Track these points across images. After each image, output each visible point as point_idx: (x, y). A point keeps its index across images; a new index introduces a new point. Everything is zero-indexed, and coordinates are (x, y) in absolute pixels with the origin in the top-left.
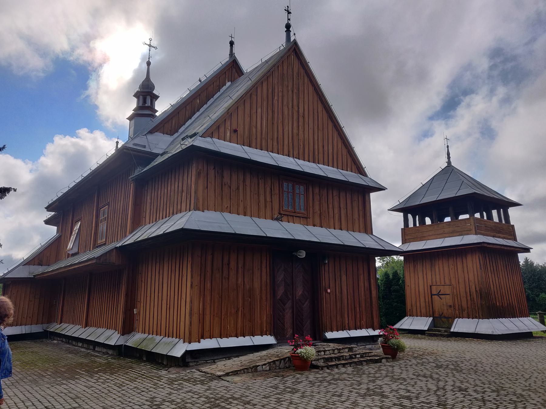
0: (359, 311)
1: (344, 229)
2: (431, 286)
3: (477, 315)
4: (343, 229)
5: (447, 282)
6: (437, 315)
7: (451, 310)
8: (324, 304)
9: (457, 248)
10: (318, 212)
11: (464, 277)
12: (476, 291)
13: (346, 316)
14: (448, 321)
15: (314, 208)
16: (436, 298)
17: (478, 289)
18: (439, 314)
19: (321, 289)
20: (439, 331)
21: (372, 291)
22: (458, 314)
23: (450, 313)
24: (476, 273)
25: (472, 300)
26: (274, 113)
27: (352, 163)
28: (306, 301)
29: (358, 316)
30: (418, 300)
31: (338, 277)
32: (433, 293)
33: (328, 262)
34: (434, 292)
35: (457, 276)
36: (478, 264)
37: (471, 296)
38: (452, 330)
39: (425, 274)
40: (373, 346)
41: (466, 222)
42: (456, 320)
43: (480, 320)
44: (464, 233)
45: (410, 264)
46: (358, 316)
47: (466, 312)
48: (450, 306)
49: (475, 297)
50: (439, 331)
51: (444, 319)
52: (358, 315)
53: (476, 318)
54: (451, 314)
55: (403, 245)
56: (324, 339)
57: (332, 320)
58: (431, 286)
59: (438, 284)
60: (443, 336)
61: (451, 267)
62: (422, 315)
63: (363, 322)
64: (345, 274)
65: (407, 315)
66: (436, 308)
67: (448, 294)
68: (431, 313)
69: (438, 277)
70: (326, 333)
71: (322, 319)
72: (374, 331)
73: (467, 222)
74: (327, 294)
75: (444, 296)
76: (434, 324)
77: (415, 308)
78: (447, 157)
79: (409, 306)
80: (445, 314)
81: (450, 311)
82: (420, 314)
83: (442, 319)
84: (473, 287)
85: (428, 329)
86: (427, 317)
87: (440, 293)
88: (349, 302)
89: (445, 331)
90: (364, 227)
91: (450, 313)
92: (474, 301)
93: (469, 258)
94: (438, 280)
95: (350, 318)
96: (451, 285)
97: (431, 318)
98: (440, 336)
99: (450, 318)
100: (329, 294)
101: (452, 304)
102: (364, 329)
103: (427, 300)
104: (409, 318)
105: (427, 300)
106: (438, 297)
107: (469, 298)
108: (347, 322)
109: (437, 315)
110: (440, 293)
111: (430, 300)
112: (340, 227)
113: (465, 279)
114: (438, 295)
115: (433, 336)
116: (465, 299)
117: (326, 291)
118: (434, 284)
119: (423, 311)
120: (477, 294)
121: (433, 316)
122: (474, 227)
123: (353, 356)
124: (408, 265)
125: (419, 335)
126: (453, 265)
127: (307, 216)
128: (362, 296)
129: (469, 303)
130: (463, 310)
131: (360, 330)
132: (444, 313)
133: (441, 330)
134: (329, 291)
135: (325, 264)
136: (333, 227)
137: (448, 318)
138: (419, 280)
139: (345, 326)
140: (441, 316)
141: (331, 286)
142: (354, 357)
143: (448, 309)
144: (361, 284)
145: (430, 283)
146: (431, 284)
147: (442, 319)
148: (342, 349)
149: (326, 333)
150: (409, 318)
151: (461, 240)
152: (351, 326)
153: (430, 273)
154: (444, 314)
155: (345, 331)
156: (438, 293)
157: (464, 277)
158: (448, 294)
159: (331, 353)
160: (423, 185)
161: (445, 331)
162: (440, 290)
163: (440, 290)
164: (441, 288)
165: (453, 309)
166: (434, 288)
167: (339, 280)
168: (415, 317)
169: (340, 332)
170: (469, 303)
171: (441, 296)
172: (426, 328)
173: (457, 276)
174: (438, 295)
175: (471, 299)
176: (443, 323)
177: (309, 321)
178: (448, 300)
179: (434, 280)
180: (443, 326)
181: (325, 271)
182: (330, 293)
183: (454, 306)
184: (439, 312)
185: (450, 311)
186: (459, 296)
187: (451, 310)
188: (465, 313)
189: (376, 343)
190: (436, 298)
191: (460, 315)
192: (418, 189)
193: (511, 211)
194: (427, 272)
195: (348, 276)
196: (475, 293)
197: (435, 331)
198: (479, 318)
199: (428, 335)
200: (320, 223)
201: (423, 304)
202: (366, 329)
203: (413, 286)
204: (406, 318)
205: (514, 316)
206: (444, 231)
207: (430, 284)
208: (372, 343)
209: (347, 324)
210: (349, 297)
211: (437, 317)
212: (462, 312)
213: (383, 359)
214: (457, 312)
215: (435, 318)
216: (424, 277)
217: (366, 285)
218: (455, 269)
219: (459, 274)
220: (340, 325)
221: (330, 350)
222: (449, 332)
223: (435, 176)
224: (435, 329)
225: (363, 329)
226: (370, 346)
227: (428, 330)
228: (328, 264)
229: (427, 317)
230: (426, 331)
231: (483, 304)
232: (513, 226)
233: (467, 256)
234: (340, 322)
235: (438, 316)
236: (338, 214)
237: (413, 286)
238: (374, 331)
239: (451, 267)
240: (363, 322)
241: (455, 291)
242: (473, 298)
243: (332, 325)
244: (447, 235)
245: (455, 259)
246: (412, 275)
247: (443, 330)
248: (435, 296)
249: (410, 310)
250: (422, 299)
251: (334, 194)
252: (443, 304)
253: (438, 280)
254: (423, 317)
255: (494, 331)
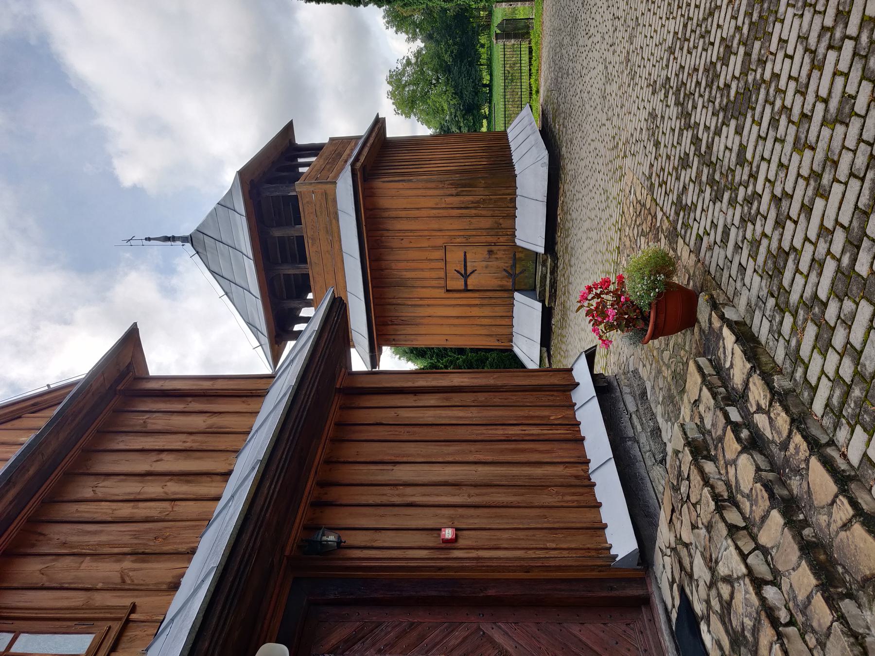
0: (520, 428)
1: (230, 464)
2: (448, 291)
3: (509, 197)
4: (231, 468)
5: (439, 254)
6: (509, 283)
7: (498, 252)
8: (500, 559)
9: (364, 224)
10: (127, 564)
11: (427, 217)
12: (457, 195)
13: (539, 471)
14: (521, 259)
15: (100, 585)
16: (472, 282)
17: (454, 191)
18: (507, 277)
19: (440, 569)
20: (544, 277)
21: (450, 384)
22: (506, 238)
23: (503, 254)
24: (420, 192)
25: (476, 205)
26: (529, 489)
27: (17, 423)
28: (491, 641)
29: (535, 431)
30: (478, 321)
31: (398, 495)
32: (463, 287)
33: (333, 529)
34: (459, 284)
35: (426, 233)
36: (400, 185)
37: (470, 206)
38: (541, 250)
39: (421, 302)
40: (626, 390)
41: (308, 202)
42: (518, 243)
43: (518, 192)
44: (332, 210)
45: (399, 333)
46: (535, 431)
47: (501, 221)
48: (490, 252)
49: (470, 198)
50: (544, 277)
51: (517, 269)
52: (531, 432)
53: (513, 201)
54: (507, 253)
55: (355, 344)
56: (638, 565)
57: (562, 525)
58: (448, 291)
59: (442, 274)
60: (556, 269)
61: (405, 243)
62: (509, 314)
63: (552, 418)
64: (390, 467)
65: (508, 348)
66: (494, 283)
67: (465, 255)
68: (505, 295)
69: (426, 274)
70: (613, 552)
71: (559, 568)
72: (578, 384)
73: (307, 200)
74: (462, 543)
75: (468, 264)
76: (529, 291)
77: (494, 329)
78: (173, 243)
79: (491, 343)
80: (506, 265)
81: (500, 255)
82: (507, 320)
83: (517, 272)
84: (449, 200)
85: (539, 301)
86: (513, 304)
87: (463, 272)
88: (490, 458)
89: (543, 266)
90: (244, 399)
91: (503, 254)
92: (478, 202)
93: (385, 202)
94: (434, 274)
95: (546, 458)
96: (445, 246)
97: (517, 295)
98: (556, 274)
99: (515, 255)
100: (460, 533)
101: (487, 248)
102: (577, 416)
103: (477, 302)
104: (515, 344)
105: (477, 302)
106: (470, 277)
107: (473, 212)
108: (559, 470)
109: (509, 283)
110: (463, 272)
111: (477, 295)
112: (219, 477)
113: (433, 215)
114: (466, 276)
115: (556, 291)
116: (474, 220)
117: (449, 545)
118: (442, 282)
119: (500, 311)
120: (465, 193)
121: (511, 290)
122: (320, 186)
123: (743, 435)
124: (402, 337)
125: (553, 322)
126: (402, 239)
127: (119, 619)
128: (470, 415)
129: (484, 212)
130: (498, 226)
131: (581, 426)
132: (504, 268)
133: (542, 274)
134: (448, 533)
135: (339, 543)
136: (211, 503)
137: (514, 258)
138: (435, 315)
139: (577, 477)
140: (511, 274)
141: (430, 523)
142: (745, 434)
143: (497, 258)
144: (429, 416)
145: (441, 293)
146: (443, 291)
147: (517, 272)
148: (713, 487)
149: (613, 552)
150: (515, 344)
151: (348, 214)
152: (572, 457)
153: (419, 290)
154: (507, 267)
155: (594, 478)
156: (463, 276)
157: (427, 217)
158: (465, 255)
159: (753, 546)
160: (226, 294)
161: (544, 264)
162: (456, 270)
163: (456, 270)
164: (451, 268)
165: (494, 248)
166: (452, 285)
167: (409, 490)
168: (514, 329)
169: (600, 494)
170: (484, 212)
171: (469, 270)
172: (539, 306)
173: (426, 233)
174: (466, 276)
175: (475, 208)
176: (525, 270)
177: (575, 629)
178: (477, 258)
179: (434, 283)
180: (533, 271)
181: (369, 544)
182: (457, 529)
183: (489, 244)
184: (503, 278)
185: (500, 255)
186: (469, 233)
187: (498, 252)
188: (506, 223)
189: (616, 384)
190: (472, 282)
191: (509, 233)
192: (235, 306)
193: (302, 138)
194: (416, 296)
195: (398, 459)
196: (462, 198)
197: (543, 285)
198: (515, 194)
199: (554, 300)
200: (175, 557)
201: (487, 311)
202: (576, 408)
203: (447, 330)
204: (516, 350)
205: (509, 147)
206: (327, 251)
207: (443, 290)
208: (618, 394)
209: (565, 471)
210: (471, 458)
211: (514, 284)
212: (502, 228)
213: (726, 316)
214: (502, 239)
215: (516, 288)
216: (427, 304)
217: (432, 402)
218: (412, 234)
219: (422, 227)
220: (574, 494)
221: (737, 548)
222: (545, 257)
223: (209, 270)
224: (541, 286)
225: (578, 420)
226: (629, 400)
227: (543, 301)
228: (342, 533)
229: (514, 305)
230: (544, 306)
231: (485, 183)
232: (332, 139)
233: (384, 208)
234: (563, 495)
235: (511, 280)
236: (168, 484)
237: (447, 330)
238: (578, 384)
239: (405, 243)
240: (555, 416)
241: (458, 240)
242: (473, 202)
243: (578, 525)
244: (336, 246)
245: (386, 233)
246: (422, 330)
247: (542, 269)
248: (468, 283)
249: (498, 340)
250: (476, 312)
251: (88, 493)
252: (487, 267)
253: (434, 274)
254: (513, 312)
255: (541, 162)
